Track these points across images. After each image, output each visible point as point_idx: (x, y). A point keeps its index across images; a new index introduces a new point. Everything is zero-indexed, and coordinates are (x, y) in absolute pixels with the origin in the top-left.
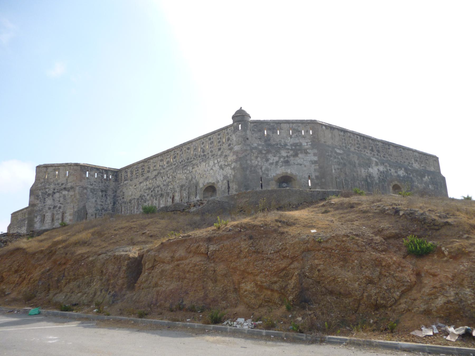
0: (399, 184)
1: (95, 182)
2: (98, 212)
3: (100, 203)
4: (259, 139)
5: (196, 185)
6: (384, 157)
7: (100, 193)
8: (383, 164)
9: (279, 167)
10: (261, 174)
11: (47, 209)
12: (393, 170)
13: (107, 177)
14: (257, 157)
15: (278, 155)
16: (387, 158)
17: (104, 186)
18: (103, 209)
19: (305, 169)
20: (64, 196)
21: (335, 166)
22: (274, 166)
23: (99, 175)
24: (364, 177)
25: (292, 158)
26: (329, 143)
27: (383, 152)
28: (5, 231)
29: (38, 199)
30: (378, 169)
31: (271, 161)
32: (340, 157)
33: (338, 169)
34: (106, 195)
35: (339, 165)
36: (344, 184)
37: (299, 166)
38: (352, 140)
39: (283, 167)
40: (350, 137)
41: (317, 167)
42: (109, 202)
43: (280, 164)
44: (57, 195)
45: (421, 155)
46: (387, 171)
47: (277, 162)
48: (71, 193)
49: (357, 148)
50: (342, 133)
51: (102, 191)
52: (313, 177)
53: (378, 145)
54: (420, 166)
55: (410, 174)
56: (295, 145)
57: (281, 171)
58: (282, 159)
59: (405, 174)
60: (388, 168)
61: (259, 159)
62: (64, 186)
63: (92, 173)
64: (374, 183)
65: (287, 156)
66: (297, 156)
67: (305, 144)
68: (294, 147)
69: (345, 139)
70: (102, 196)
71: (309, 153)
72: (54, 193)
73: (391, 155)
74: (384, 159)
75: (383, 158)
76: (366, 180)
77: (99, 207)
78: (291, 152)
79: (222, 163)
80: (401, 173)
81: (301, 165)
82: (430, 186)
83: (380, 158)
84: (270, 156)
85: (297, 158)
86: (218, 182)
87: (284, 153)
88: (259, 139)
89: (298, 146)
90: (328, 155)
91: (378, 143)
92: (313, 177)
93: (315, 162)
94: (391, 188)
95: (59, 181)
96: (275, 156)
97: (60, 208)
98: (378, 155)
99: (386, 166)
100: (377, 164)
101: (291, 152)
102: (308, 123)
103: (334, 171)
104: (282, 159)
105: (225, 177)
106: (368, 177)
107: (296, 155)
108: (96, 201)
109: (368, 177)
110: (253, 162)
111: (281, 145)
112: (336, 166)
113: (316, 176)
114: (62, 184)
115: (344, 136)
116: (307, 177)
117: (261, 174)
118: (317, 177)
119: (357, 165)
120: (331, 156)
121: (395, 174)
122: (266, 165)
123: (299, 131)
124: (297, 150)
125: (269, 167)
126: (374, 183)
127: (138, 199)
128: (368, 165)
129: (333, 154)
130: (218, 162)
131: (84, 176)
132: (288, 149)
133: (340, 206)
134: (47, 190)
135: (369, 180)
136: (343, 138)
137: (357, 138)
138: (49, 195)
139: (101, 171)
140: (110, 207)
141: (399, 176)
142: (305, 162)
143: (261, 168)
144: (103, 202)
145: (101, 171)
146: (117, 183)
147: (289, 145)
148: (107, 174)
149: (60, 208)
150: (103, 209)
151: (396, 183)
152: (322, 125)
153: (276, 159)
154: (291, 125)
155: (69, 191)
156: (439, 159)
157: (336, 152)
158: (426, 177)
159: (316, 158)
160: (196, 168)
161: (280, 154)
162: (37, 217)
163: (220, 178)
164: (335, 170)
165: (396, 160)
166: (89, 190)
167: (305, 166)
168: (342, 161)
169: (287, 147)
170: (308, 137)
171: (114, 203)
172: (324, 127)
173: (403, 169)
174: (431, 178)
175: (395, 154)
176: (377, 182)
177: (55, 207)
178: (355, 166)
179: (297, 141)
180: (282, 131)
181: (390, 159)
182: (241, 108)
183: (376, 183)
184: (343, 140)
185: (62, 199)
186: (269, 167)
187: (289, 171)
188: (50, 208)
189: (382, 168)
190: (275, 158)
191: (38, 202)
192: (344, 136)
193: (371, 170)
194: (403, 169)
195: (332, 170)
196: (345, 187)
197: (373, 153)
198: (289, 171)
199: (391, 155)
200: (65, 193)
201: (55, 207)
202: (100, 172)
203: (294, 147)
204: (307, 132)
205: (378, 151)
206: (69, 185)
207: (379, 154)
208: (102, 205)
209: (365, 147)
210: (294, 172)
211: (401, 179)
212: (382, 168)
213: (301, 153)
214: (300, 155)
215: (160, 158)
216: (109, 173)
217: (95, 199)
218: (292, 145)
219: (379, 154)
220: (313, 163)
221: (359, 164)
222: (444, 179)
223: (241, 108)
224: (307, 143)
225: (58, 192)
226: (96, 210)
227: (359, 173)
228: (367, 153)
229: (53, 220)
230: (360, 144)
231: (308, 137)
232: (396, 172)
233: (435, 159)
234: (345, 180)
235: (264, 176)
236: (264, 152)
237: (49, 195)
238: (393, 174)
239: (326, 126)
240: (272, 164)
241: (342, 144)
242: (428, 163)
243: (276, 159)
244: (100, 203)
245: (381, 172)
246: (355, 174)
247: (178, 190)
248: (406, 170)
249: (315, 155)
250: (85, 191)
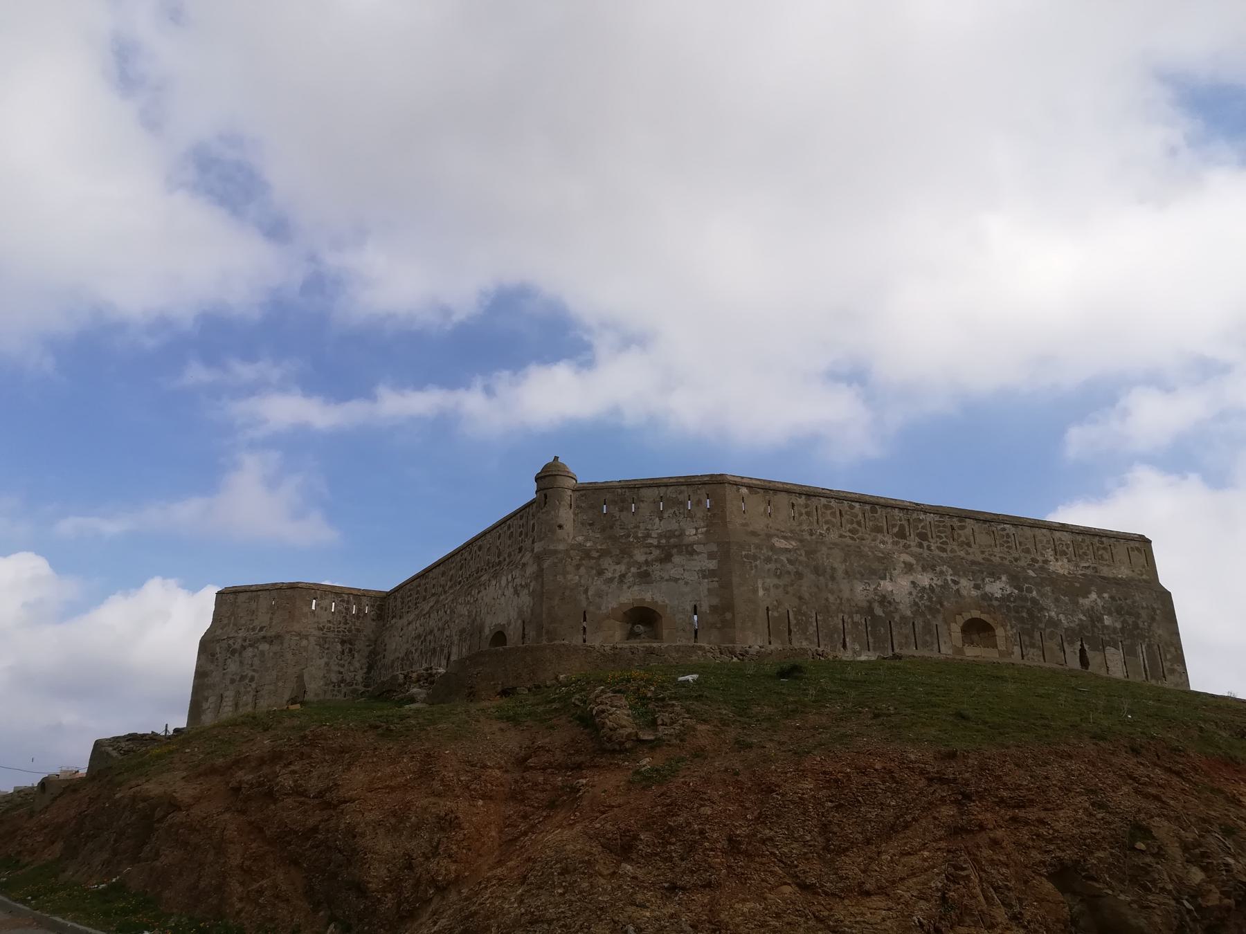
0: (984, 617)
1: (329, 622)
2: (331, 687)
3: (336, 668)
4: (590, 525)
5: (481, 629)
6: (944, 550)
7: (339, 647)
8: (929, 566)
9: (625, 587)
10: (584, 604)
11: (228, 682)
12: (965, 584)
13: (359, 610)
14: (578, 567)
15: (625, 561)
16: (953, 551)
17: (350, 631)
18: (343, 681)
19: (687, 589)
20: (262, 653)
21: (768, 580)
22: (615, 585)
23: (341, 608)
24: (865, 604)
25: (657, 566)
26: (759, 524)
27: (940, 538)
28: (181, 722)
29: (212, 662)
30: (913, 582)
31: (609, 575)
32: (783, 558)
33: (777, 587)
34: (351, 650)
35: (779, 577)
36: (793, 621)
37: (673, 584)
38: (833, 514)
39: (636, 588)
40: (826, 507)
41: (716, 585)
42: (357, 665)
43: (629, 578)
44: (249, 652)
45: (1080, 538)
46: (945, 586)
47: (623, 576)
48: (276, 648)
49: (848, 534)
50: (802, 500)
51: (343, 642)
52: (705, 607)
53: (921, 521)
54: (1077, 566)
55: (1029, 590)
56: (669, 535)
57: (631, 595)
58: (633, 570)
59: (1009, 590)
60: (949, 578)
61: (582, 570)
62: (262, 634)
63: (325, 603)
64: (897, 618)
65: (646, 562)
66: (670, 561)
67: (692, 533)
68: (663, 541)
69: (808, 514)
70: (343, 653)
71: (698, 554)
72: (244, 648)
73: (969, 545)
74: (944, 555)
75: (937, 552)
76: (870, 610)
77: (334, 677)
78: (656, 553)
79: (518, 581)
80: (997, 588)
81: (676, 580)
82: (1107, 620)
83: (926, 553)
84: (607, 563)
85: (669, 566)
86: (509, 624)
87: (640, 556)
88: (590, 525)
89: (675, 536)
90: (747, 556)
91: (922, 517)
92: (705, 607)
93: (712, 573)
94: (956, 628)
95: (256, 623)
96: (618, 564)
97: (252, 679)
98: (920, 546)
99: (942, 572)
100: (909, 568)
101: (656, 553)
102: (704, 484)
103: (761, 593)
104: (633, 570)
105: (520, 612)
106: (876, 605)
107: (666, 558)
108: (327, 664)
109: (876, 605)
110: (569, 577)
111: (636, 537)
112: (771, 581)
113: (711, 606)
114: (261, 629)
115: (806, 506)
116: (689, 608)
117: (584, 604)
118: (714, 609)
119: (840, 574)
120: (755, 558)
121: (974, 593)
122: (599, 583)
123: (681, 503)
124: (672, 547)
125: (603, 587)
126: (897, 618)
127: (403, 659)
128: (881, 568)
129: (765, 551)
130: (513, 579)
131: (305, 609)
132: (651, 545)
133: (554, 701)
134: (231, 642)
135: (879, 611)
136: (804, 511)
137: (852, 507)
138: (233, 652)
139: (346, 597)
140: (359, 678)
141: (987, 597)
142: (686, 575)
143: (586, 591)
144: (343, 666)
145: (346, 597)
146: (381, 623)
147: (654, 535)
148: (359, 604)
149: (252, 679)
150: (343, 681)
151: (976, 614)
152: (737, 483)
153: (622, 568)
154: (663, 490)
155: (271, 643)
156: (1155, 547)
157: (772, 548)
158: (1094, 596)
159: (712, 565)
160: (484, 592)
161: (631, 557)
162: (207, 700)
163: (513, 614)
164: (765, 589)
165: (986, 555)
166: (312, 639)
167: (686, 583)
168: (790, 567)
169: (650, 541)
170: (700, 514)
171: (370, 668)
172: (744, 490)
173: (1004, 578)
174: (1112, 598)
175: (983, 539)
176: (909, 613)
177: (242, 678)
178: (833, 578)
179: (674, 526)
180: (642, 505)
181: (962, 554)
182: (556, 458)
183: (903, 618)
184: (804, 517)
185: (256, 661)
186: (603, 587)
187: (648, 595)
188: (233, 681)
189: (925, 580)
190: (617, 567)
191: (212, 667)
192: (806, 506)
193: (886, 585)
194: (1004, 578)
195: (755, 591)
196: (794, 629)
197: (903, 542)
198: (648, 597)
199: (969, 545)
200: (264, 647)
201: (242, 678)
202: (343, 601)
203: (663, 541)
204: (699, 502)
205: (923, 536)
206: (272, 633)
207: (925, 544)
208: (341, 673)
209: (878, 530)
210: (659, 599)
211: (996, 603)
212: (925, 580)
213: (680, 553)
214: (677, 559)
215: (442, 568)
216: (364, 600)
217: (325, 660)
218: (660, 536)
219: (925, 544)
220: (704, 577)
221: (847, 572)
222: (1166, 597)
223: (556, 458)
224: (697, 529)
225: (250, 646)
226: (326, 684)
227: (846, 594)
228: (883, 542)
229: (236, 705)
230: (859, 523)
231: (700, 514)
232: (977, 587)
233: (1141, 546)
234: (799, 612)
235: (592, 609)
236: (595, 554)
237: (233, 652)
238: (964, 593)
239: (749, 487)
240: (611, 580)
241: (800, 524)
242: (1106, 556)
243: (622, 568)
244: (336, 668)
245: (924, 588)
246: (831, 598)
247: (456, 639)
248: (1015, 579)
249: (711, 556)
250: (304, 643)
